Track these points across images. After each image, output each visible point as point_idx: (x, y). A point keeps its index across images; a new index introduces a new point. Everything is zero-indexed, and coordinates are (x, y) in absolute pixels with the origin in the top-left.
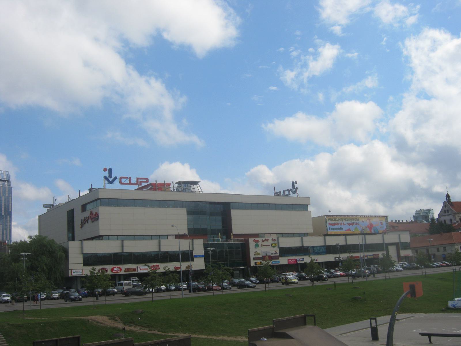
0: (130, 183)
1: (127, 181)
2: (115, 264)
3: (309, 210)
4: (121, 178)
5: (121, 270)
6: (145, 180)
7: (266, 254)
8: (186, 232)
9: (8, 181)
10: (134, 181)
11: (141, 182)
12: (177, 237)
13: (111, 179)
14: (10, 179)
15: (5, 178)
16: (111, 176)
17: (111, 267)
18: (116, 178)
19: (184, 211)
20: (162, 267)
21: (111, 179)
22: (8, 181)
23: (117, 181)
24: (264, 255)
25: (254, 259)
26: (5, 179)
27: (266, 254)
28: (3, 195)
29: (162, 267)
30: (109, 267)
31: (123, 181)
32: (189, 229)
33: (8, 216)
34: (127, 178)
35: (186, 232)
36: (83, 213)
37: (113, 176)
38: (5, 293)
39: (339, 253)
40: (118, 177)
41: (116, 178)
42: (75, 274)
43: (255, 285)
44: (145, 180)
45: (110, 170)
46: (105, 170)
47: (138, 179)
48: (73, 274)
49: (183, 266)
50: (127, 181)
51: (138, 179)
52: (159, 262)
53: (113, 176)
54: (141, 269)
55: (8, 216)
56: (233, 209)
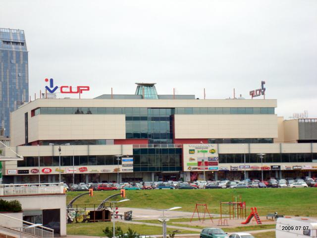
0: (71, 92)
1: (68, 90)
2: (46, 165)
3: (275, 113)
4: (62, 88)
5: (51, 170)
6: (86, 88)
7: (203, 160)
8: (124, 137)
9: (23, 44)
10: (75, 89)
11: (82, 90)
12: (117, 142)
13: (52, 89)
14: (25, 41)
15: (19, 40)
16: (52, 86)
17: (42, 168)
18: (57, 88)
19: (123, 117)
20: (91, 169)
21: (52, 89)
22: (23, 44)
23: (58, 90)
24: (201, 160)
25: (188, 164)
26: (19, 41)
27: (203, 160)
28: (17, 62)
29: (91, 169)
30: (40, 168)
31: (64, 90)
32: (127, 134)
33: (25, 90)
34: (67, 87)
35: (124, 137)
36: (33, 117)
37: (54, 86)
38: (26, 181)
39: (74, 176)
40: (60, 86)
41: (57, 88)
42: (10, 173)
43: (192, 184)
44: (86, 88)
45: (52, 81)
46: (47, 80)
47: (78, 87)
48: (9, 173)
49: (110, 169)
50: (68, 90)
51: (78, 87)
52: (86, 165)
53: (54, 86)
54: (69, 171)
55: (25, 90)
56: (177, 114)
